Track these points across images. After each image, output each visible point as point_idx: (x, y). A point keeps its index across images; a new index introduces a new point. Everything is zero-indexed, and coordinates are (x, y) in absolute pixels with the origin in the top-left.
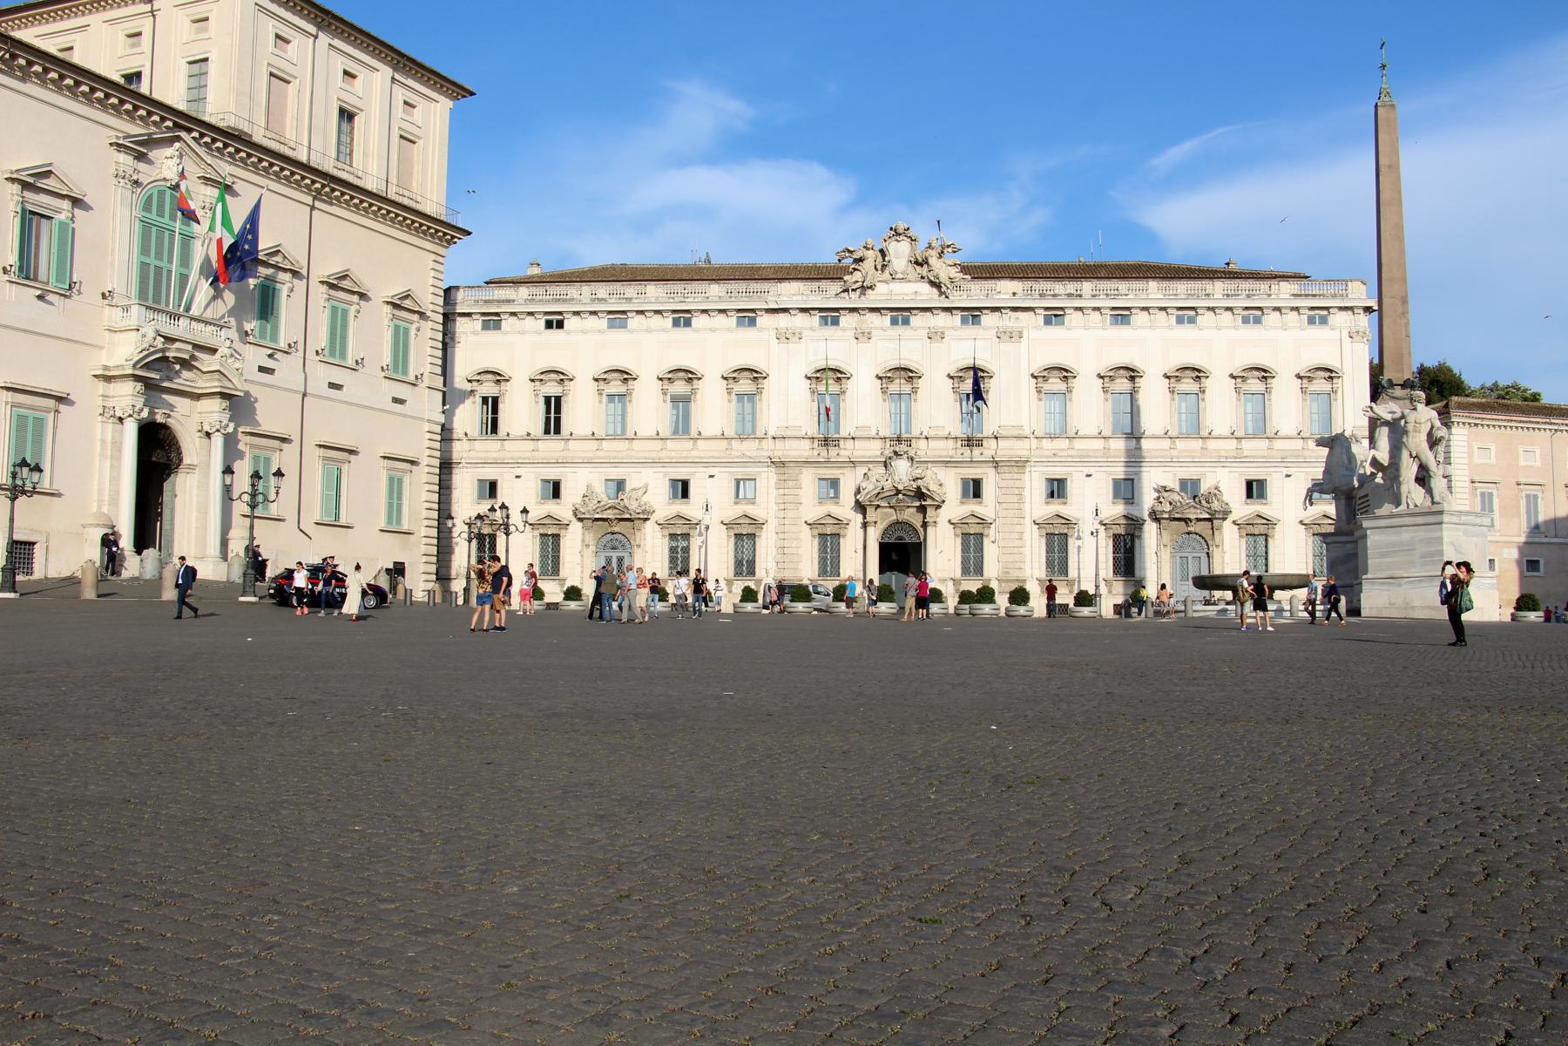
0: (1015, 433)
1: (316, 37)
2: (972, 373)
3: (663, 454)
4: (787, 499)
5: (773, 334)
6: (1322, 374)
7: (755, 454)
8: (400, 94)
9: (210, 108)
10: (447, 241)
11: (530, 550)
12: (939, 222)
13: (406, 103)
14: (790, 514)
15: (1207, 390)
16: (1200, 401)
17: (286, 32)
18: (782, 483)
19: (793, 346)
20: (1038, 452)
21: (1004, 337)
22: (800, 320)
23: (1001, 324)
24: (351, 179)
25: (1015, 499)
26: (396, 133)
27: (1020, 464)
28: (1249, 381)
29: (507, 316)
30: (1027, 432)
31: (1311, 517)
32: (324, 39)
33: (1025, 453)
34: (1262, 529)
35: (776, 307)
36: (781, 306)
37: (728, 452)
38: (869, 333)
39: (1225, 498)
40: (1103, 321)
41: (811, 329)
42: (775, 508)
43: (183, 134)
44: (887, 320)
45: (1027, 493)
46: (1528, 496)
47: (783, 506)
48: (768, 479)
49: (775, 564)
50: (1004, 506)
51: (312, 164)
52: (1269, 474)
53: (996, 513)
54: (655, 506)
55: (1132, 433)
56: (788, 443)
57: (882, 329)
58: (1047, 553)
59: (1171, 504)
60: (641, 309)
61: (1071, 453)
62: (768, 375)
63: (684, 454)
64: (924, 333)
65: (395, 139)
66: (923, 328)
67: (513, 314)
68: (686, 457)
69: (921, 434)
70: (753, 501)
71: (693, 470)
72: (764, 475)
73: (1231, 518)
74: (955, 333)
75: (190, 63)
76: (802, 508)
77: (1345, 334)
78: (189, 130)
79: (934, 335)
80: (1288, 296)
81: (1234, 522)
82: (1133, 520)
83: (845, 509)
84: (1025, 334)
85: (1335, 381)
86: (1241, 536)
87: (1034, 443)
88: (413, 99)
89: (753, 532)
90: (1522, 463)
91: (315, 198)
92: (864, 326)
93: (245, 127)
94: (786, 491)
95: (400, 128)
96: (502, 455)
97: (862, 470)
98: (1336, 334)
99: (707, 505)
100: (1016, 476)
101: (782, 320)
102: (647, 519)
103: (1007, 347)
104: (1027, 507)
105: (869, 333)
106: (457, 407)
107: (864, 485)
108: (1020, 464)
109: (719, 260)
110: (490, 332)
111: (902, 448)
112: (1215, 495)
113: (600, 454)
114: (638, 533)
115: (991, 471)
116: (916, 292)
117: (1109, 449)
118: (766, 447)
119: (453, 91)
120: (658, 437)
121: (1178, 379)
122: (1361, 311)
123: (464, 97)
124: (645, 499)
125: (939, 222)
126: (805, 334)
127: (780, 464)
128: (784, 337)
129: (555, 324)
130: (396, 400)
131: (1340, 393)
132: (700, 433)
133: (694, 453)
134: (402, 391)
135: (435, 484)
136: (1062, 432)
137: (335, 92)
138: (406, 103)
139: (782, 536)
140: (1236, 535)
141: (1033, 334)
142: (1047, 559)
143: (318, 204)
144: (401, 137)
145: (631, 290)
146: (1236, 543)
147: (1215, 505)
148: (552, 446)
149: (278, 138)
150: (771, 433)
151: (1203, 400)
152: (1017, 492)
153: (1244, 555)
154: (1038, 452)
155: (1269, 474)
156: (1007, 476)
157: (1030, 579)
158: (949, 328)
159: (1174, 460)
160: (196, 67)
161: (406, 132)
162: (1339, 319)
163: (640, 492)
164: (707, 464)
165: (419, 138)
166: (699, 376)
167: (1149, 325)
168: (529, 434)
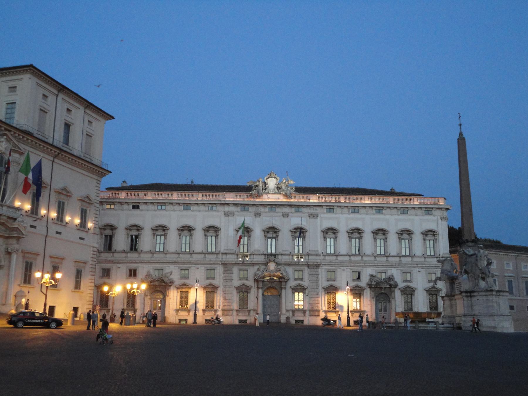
0: (315, 253)
1: (57, 95)
2: (299, 230)
3: (179, 259)
4: (227, 278)
5: (223, 213)
6: (431, 233)
7: (215, 260)
8: (87, 118)
9: (15, 122)
10: (102, 175)
11: (202, 298)
12: (287, 172)
13: (89, 121)
14: (228, 284)
15: (388, 238)
16: (385, 242)
17: (47, 93)
18: (225, 271)
19: (231, 218)
20: (324, 261)
21: (312, 217)
22: (233, 209)
23: (310, 211)
24: (69, 151)
25: (315, 279)
26: (85, 133)
27: (317, 266)
28: (403, 235)
29: (142, 204)
30: (320, 252)
31: (403, 287)
32: (61, 96)
33: (319, 261)
34: (410, 292)
35: (225, 203)
36: (226, 203)
37: (204, 259)
38: (260, 214)
39: (396, 280)
40: (349, 211)
41: (238, 212)
42: (222, 281)
43: (7, 133)
44: (182, 208)
45: (320, 276)
46: (509, 281)
47: (226, 280)
48: (220, 270)
49: (222, 304)
50: (311, 281)
51: (55, 144)
52: (138, 267)
53: (308, 284)
54: (175, 280)
55: (384, 255)
56: (228, 256)
57: (264, 212)
58: (180, 299)
59: (375, 282)
60: (197, 202)
61: (337, 261)
62: (169, 228)
63: (187, 260)
64: (281, 214)
65: (85, 136)
66: (281, 212)
67: (146, 203)
68: (188, 261)
69: (439, 255)
70: (214, 279)
71: (190, 266)
72: (218, 268)
73: (398, 287)
74: (265, 214)
75: (8, 104)
76: (234, 281)
77: (439, 218)
78: (10, 131)
79: (285, 215)
80: (99, 202)
81: (399, 289)
82: (361, 288)
83: (250, 283)
84: (319, 215)
85: (436, 236)
86: (402, 295)
87: (322, 257)
88: (91, 119)
89: (214, 291)
90: (506, 268)
91: (54, 158)
92: (258, 211)
93: (30, 130)
94: (227, 275)
95: (86, 131)
96: (112, 259)
97: (256, 267)
98: (435, 218)
99: (197, 280)
100: (316, 270)
101: (227, 209)
102: (172, 285)
103: (312, 220)
104: (320, 282)
105: (260, 214)
106: (502, 244)
107: (258, 272)
108: (317, 266)
109: (196, 182)
110: (135, 210)
111: (272, 258)
112: (392, 278)
113: (153, 259)
114: (393, 294)
115: (306, 268)
116: (278, 198)
117: (351, 260)
118: (219, 257)
119: (107, 117)
120: (124, 252)
121: (105, 229)
122: (445, 210)
123: (110, 119)
124: (171, 277)
125: (287, 172)
126: (236, 213)
127: (225, 264)
128: (227, 214)
129: (136, 207)
130: (81, 238)
131: (437, 240)
132: (194, 251)
133: (191, 259)
134: (83, 235)
135: (244, 276)
136: (360, 253)
137: (62, 117)
138: (89, 121)
139: (225, 292)
140: (400, 294)
141: (322, 215)
142: (180, 301)
143: (56, 160)
144: (87, 134)
145: (141, 194)
146: (400, 297)
147: (392, 282)
148: (133, 256)
149: (42, 135)
150: (222, 251)
151: (386, 242)
152: (316, 276)
153: (403, 302)
154: (324, 261)
155: (412, 270)
156: (312, 270)
157: (321, 310)
158: (290, 213)
159: (376, 265)
160: (9, 106)
161: (89, 133)
162: (437, 213)
163: (169, 275)
164: (196, 264)
165: (93, 135)
166: (194, 229)
167: (365, 213)
168: (124, 250)
